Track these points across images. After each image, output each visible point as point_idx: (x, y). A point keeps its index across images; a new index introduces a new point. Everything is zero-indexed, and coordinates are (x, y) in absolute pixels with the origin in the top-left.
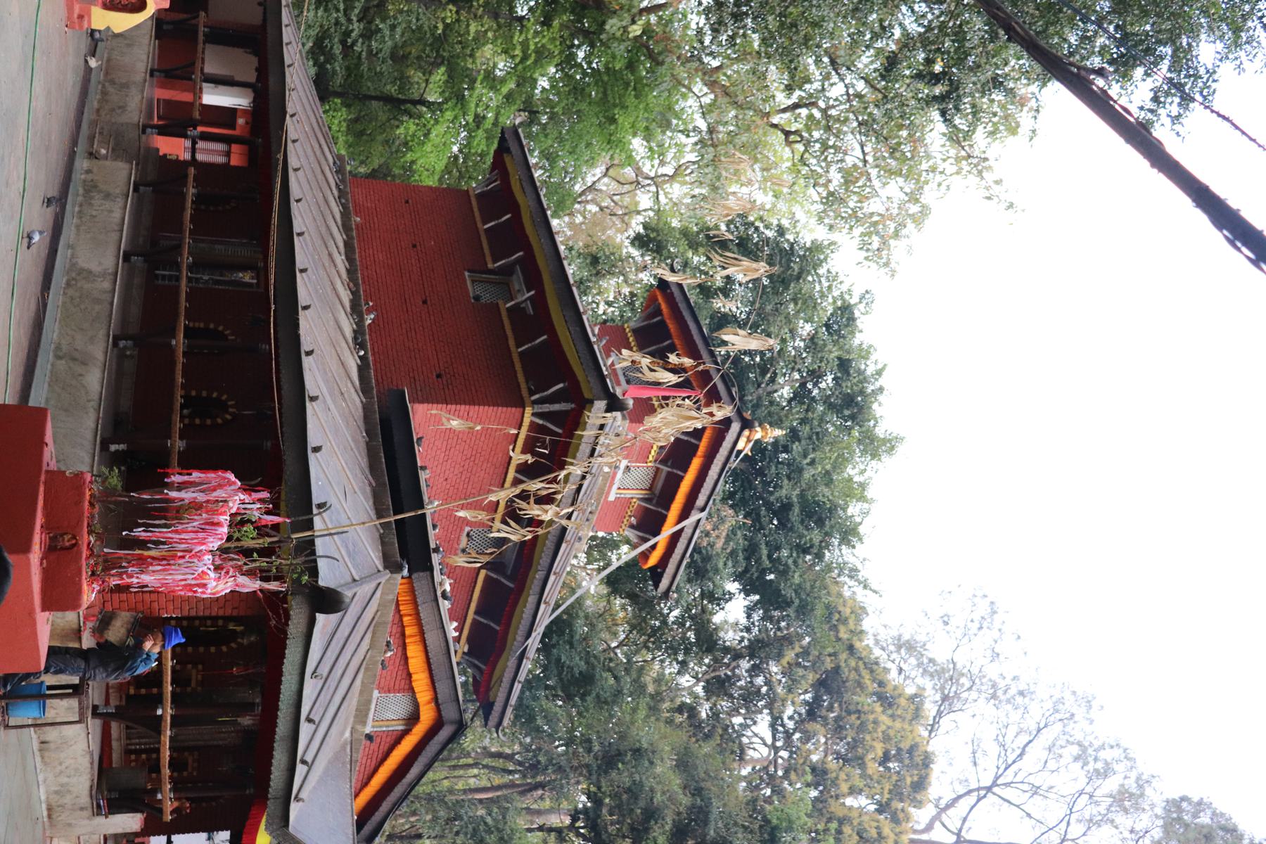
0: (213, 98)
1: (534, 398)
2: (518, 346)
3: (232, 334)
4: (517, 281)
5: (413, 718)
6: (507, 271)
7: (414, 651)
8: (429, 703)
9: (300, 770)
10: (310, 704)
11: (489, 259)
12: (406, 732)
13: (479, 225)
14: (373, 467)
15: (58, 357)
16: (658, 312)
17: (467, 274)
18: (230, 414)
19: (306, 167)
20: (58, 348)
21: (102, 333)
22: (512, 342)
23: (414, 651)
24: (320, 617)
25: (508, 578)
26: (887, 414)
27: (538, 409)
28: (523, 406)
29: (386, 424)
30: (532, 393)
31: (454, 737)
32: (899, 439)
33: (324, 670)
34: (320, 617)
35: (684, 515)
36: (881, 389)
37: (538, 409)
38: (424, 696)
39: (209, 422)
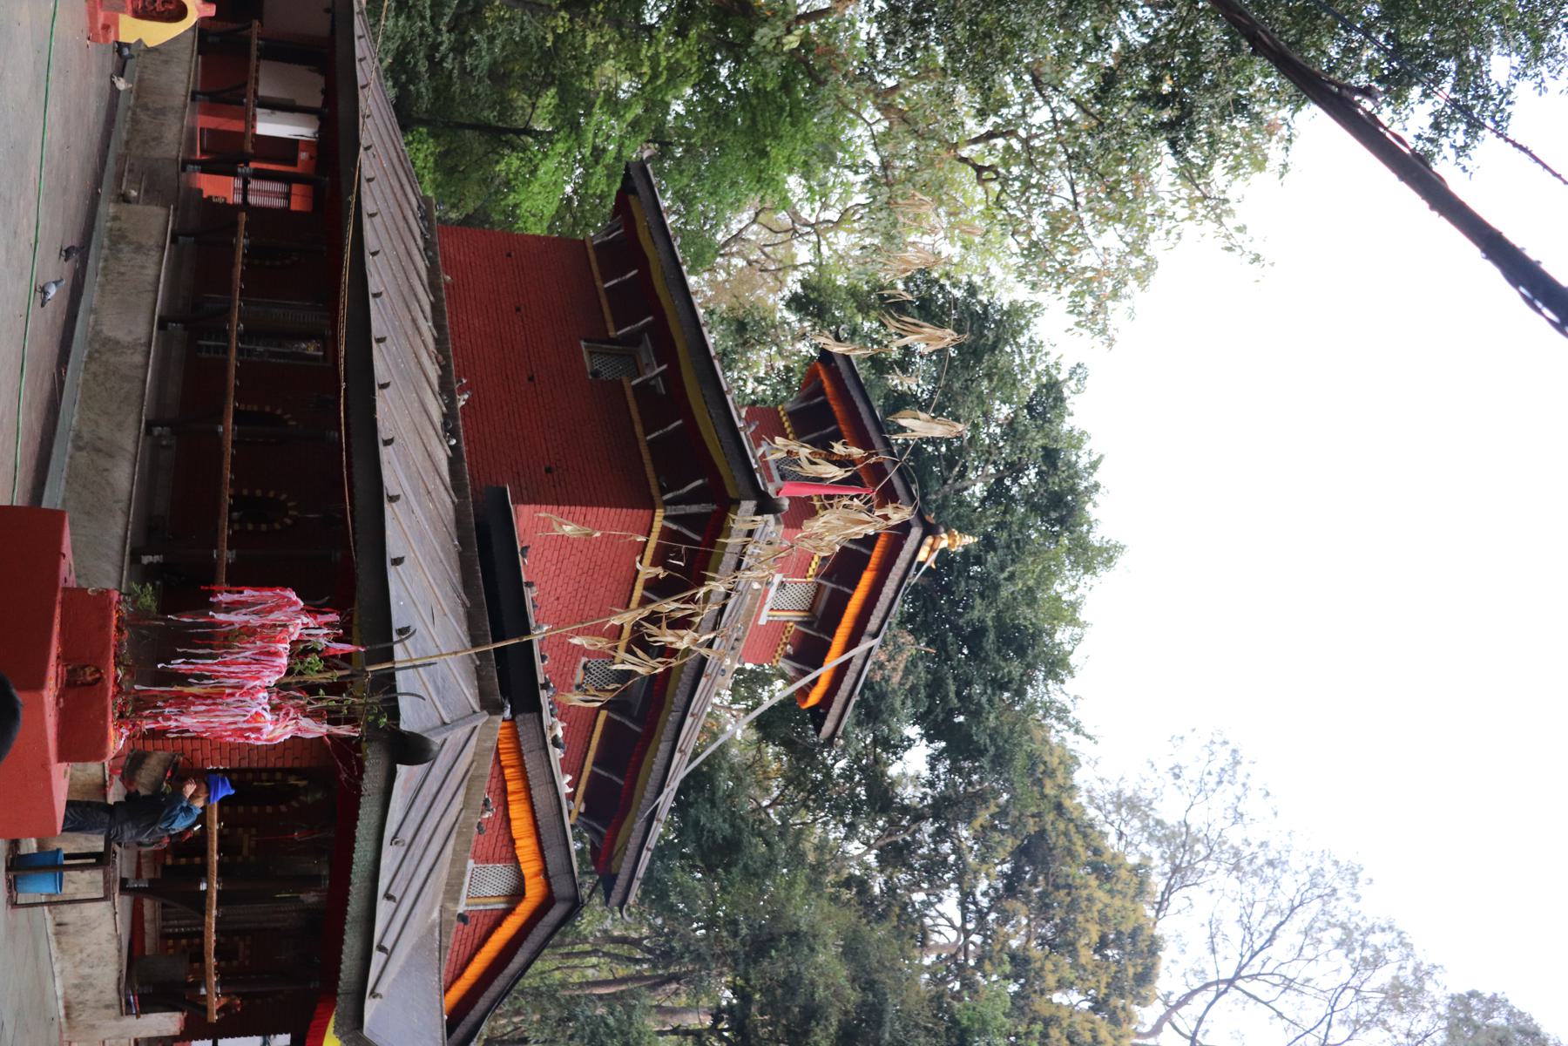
0: (270, 127)
1: (666, 497)
2: (647, 433)
4: (646, 352)
6: (633, 340)
7: (518, 812)
8: (537, 875)
9: (377, 958)
10: (390, 876)
11: (610, 325)
13: (599, 283)
15: (79, 448)
16: (820, 391)
18: (291, 517)
20: (78, 436)
21: (132, 418)
22: (639, 429)
23: (518, 812)
24: (402, 770)
26: (1104, 518)
27: (672, 511)
32: (1119, 548)
33: (407, 834)
34: (402, 770)
35: (852, 642)
36: (1096, 486)
37: (672, 511)
38: (530, 867)
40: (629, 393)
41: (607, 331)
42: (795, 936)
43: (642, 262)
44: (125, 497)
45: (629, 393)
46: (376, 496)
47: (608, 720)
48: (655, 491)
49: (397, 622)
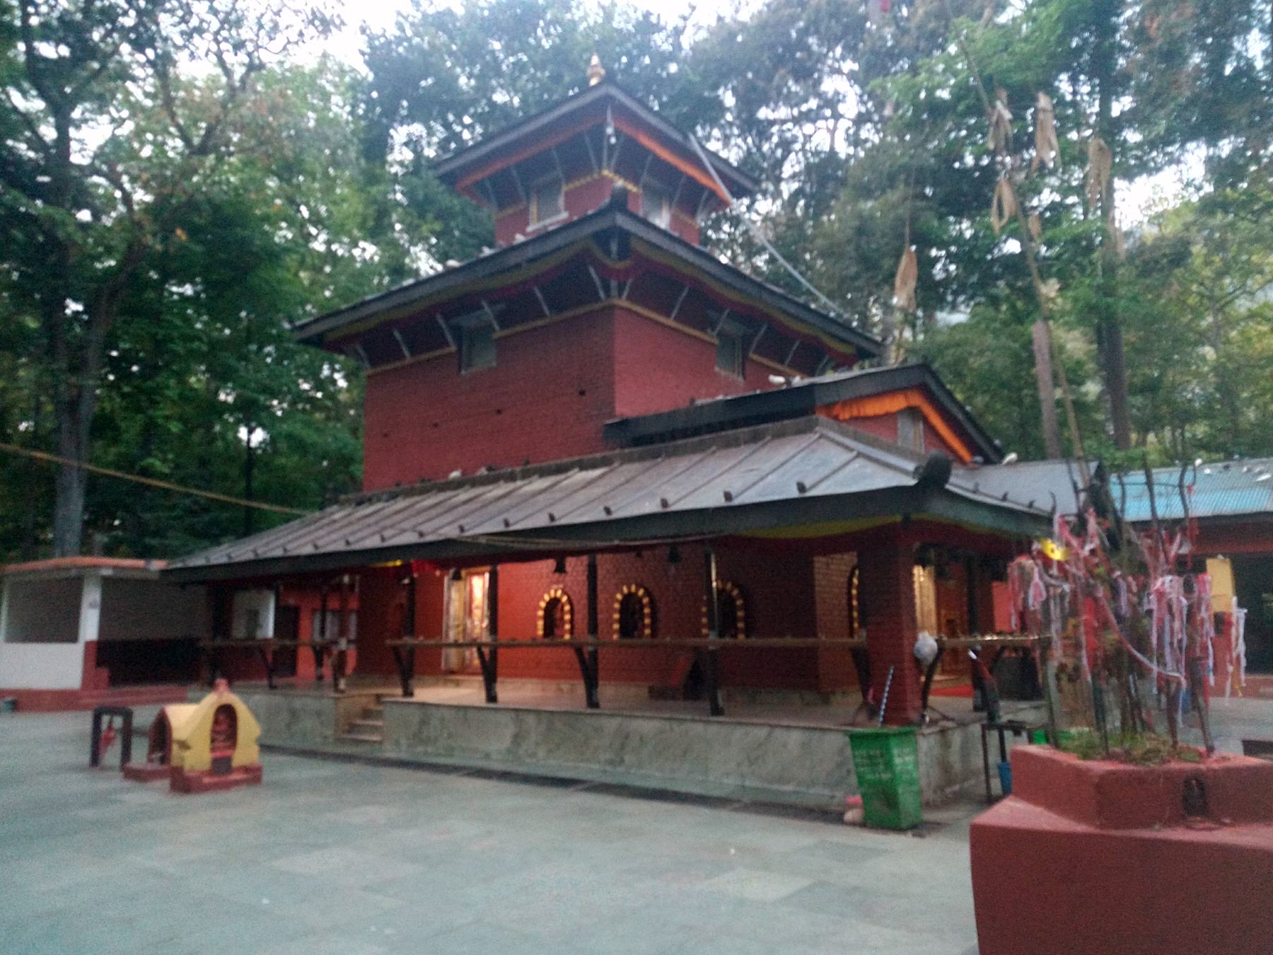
0: (268, 629)
2: (544, 316)
3: (549, 593)
4: (468, 322)
5: (913, 413)
6: (457, 332)
7: (873, 408)
8: (906, 397)
11: (446, 351)
12: (926, 420)
14: (755, 438)
15: (622, 761)
16: (479, 184)
17: (463, 372)
18: (637, 590)
19: (413, 522)
20: (611, 762)
21: (588, 721)
22: (540, 323)
25: (757, 332)
27: (614, 292)
28: (613, 307)
29: (638, 441)
30: (598, 299)
31: (934, 375)
38: (896, 404)
39: (739, 602)
40: (506, 332)
41: (450, 354)
42: (860, 231)
43: (388, 325)
44: (667, 725)
45: (506, 332)
46: (665, 517)
47: (755, 352)
48: (597, 306)
49: (794, 493)
